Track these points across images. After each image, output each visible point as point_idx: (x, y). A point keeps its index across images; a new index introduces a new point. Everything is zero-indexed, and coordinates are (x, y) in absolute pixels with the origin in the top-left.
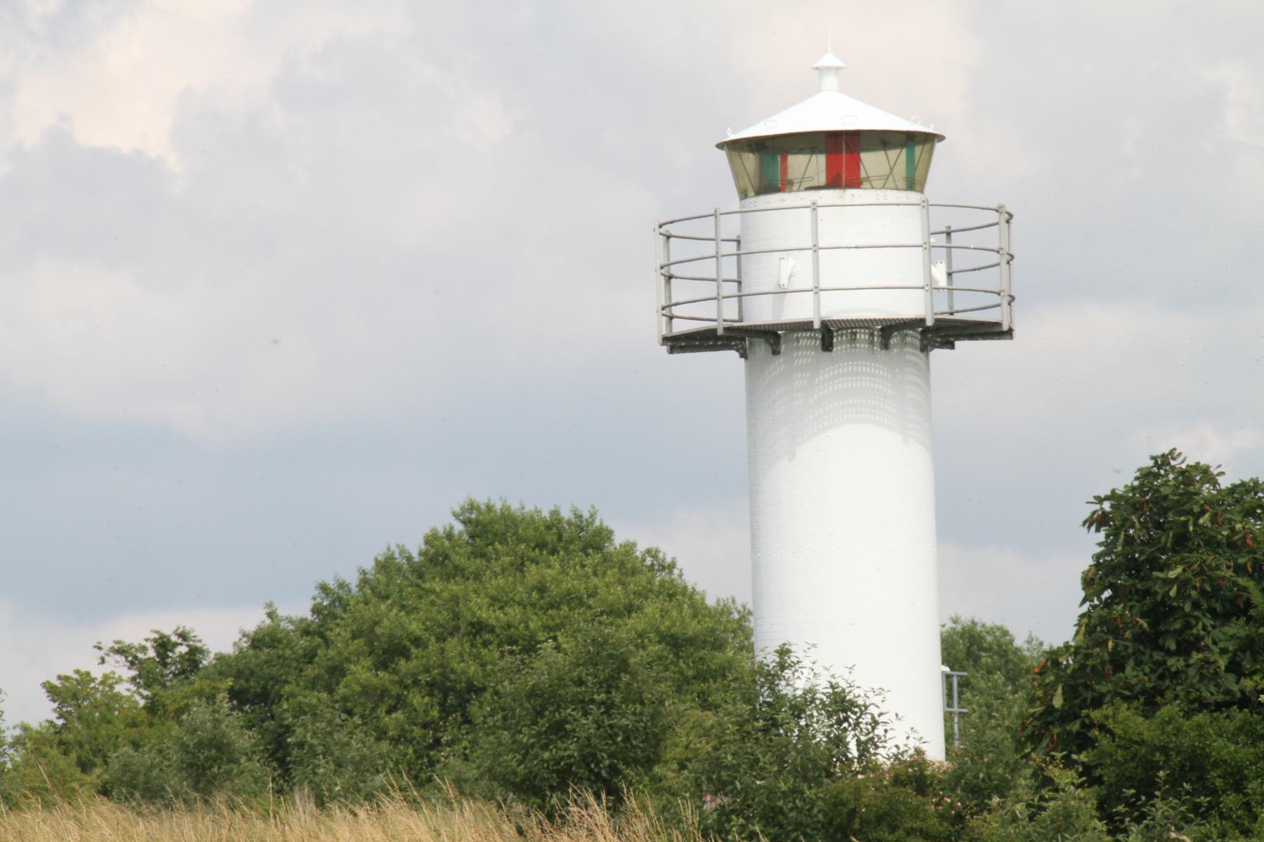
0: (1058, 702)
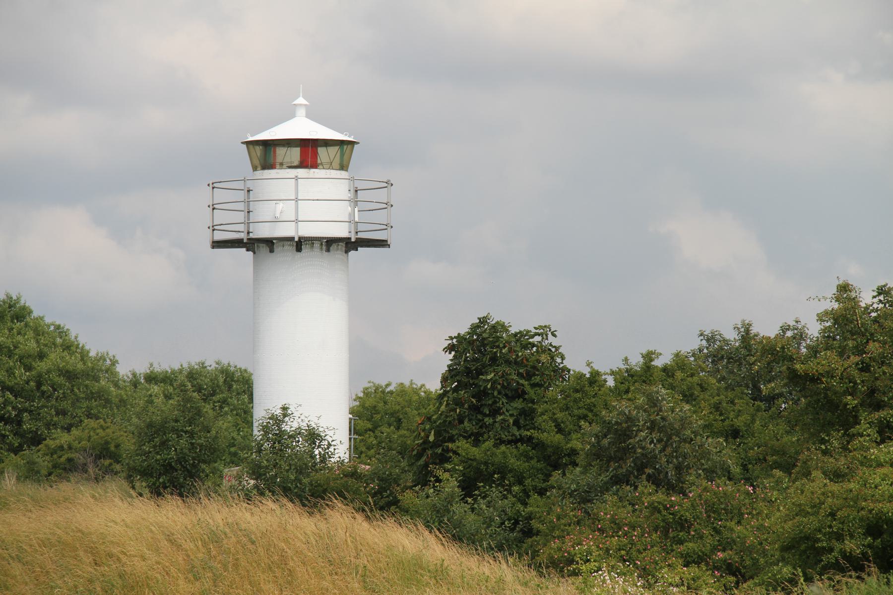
0: (431, 438)
